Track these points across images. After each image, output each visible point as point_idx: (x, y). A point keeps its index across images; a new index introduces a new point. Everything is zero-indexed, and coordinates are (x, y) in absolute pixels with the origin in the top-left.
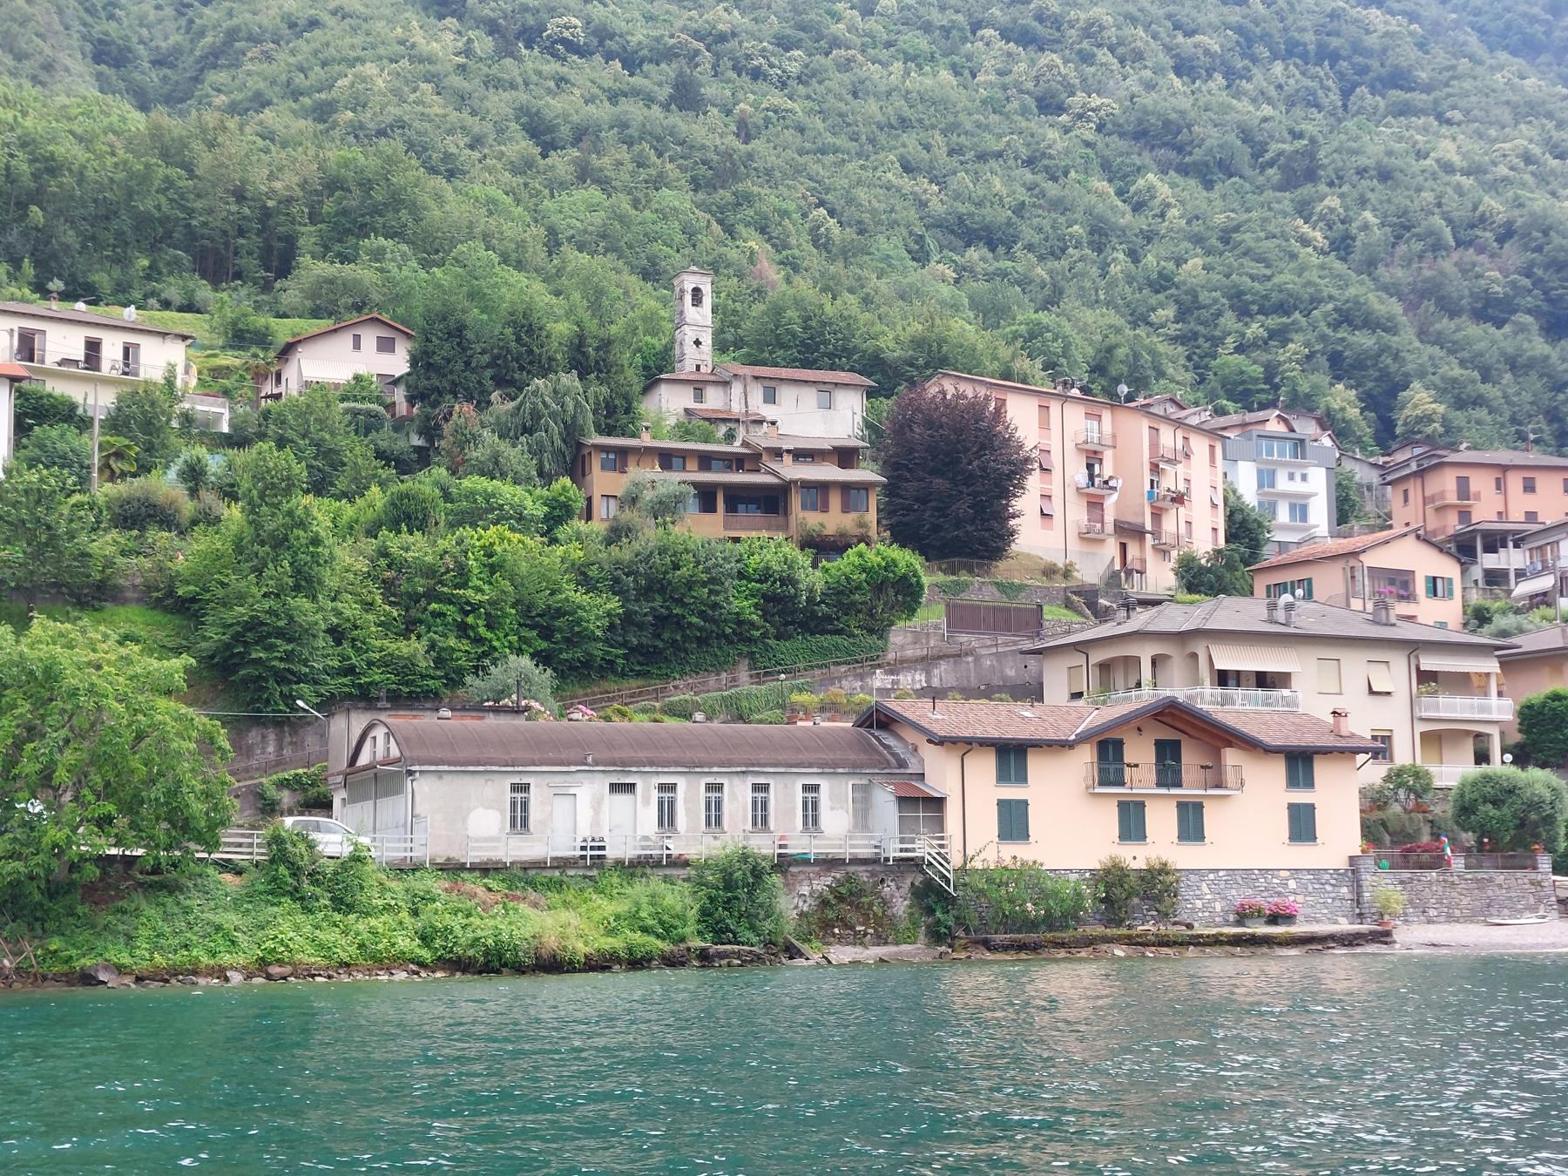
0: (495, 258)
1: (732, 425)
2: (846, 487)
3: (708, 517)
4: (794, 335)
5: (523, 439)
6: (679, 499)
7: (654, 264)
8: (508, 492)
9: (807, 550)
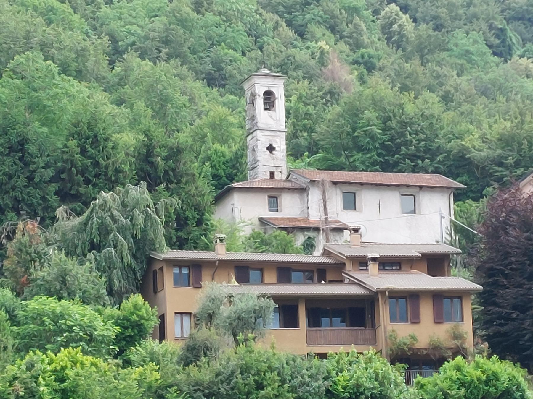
0: (55, 68)
1: (311, 234)
2: (438, 296)
3: (290, 332)
4: (373, 137)
5: (91, 256)
6: (259, 314)
7: (220, 69)
8: (76, 311)
9: (398, 365)
